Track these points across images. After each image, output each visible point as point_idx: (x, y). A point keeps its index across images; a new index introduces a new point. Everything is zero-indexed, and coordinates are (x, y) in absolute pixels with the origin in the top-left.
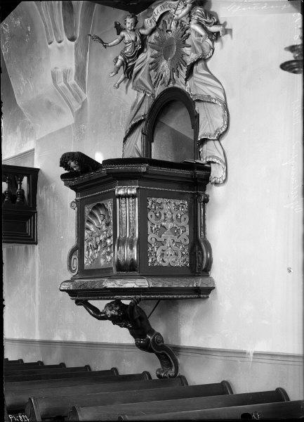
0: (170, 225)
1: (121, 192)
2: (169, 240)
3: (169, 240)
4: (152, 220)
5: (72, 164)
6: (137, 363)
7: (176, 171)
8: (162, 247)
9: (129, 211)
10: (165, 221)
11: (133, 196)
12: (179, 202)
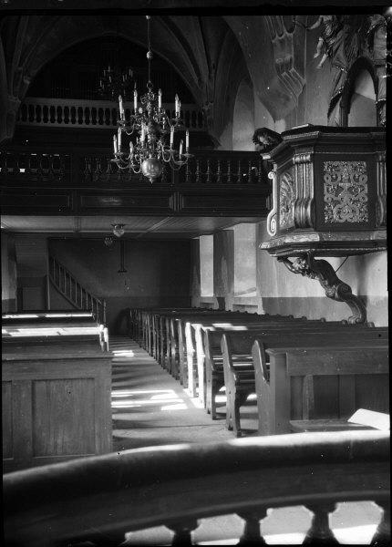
0: (347, 185)
1: (298, 159)
2: (346, 199)
3: (346, 199)
4: (329, 181)
5: (261, 139)
6: (341, 312)
7: (337, 134)
8: (338, 206)
9: (306, 174)
10: (341, 182)
11: (307, 162)
12: (357, 164)
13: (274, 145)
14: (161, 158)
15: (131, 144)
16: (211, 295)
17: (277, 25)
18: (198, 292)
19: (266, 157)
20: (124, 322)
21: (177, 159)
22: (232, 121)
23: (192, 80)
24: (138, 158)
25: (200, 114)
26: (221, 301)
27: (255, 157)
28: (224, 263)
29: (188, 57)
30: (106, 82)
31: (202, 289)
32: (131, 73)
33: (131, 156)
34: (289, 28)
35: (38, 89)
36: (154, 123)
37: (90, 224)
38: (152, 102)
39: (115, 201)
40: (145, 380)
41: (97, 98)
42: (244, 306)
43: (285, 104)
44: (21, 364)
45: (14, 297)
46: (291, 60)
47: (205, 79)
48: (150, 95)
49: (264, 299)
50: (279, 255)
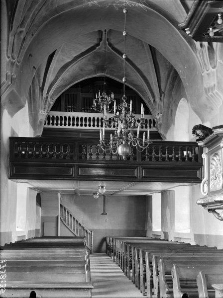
13: (207, 135)
14: (131, 144)
15: (111, 135)
16: (159, 230)
17: (205, 64)
18: (151, 228)
19: (200, 144)
20: (104, 245)
21: (141, 145)
22: (174, 124)
23: (149, 101)
24: (115, 144)
25: (154, 121)
26: (166, 234)
27: (190, 146)
28: (168, 211)
29: (147, 88)
30: (97, 102)
31: (153, 226)
32: (113, 96)
33: (111, 142)
34: (213, 66)
35: (56, 107)
36: (126, 121)
37: (84, 186)
38: (126, 108)
39: (101, 172)
40: (115, 288)
41: (93, 111)
42: (181, 238)
43: (210, 112)
44: (159, 92)
45: (39, 228)
46: (215, 85)
47: (158, 100)
48: (124, 104)
49: (195, 235)
50: (210, 208)
